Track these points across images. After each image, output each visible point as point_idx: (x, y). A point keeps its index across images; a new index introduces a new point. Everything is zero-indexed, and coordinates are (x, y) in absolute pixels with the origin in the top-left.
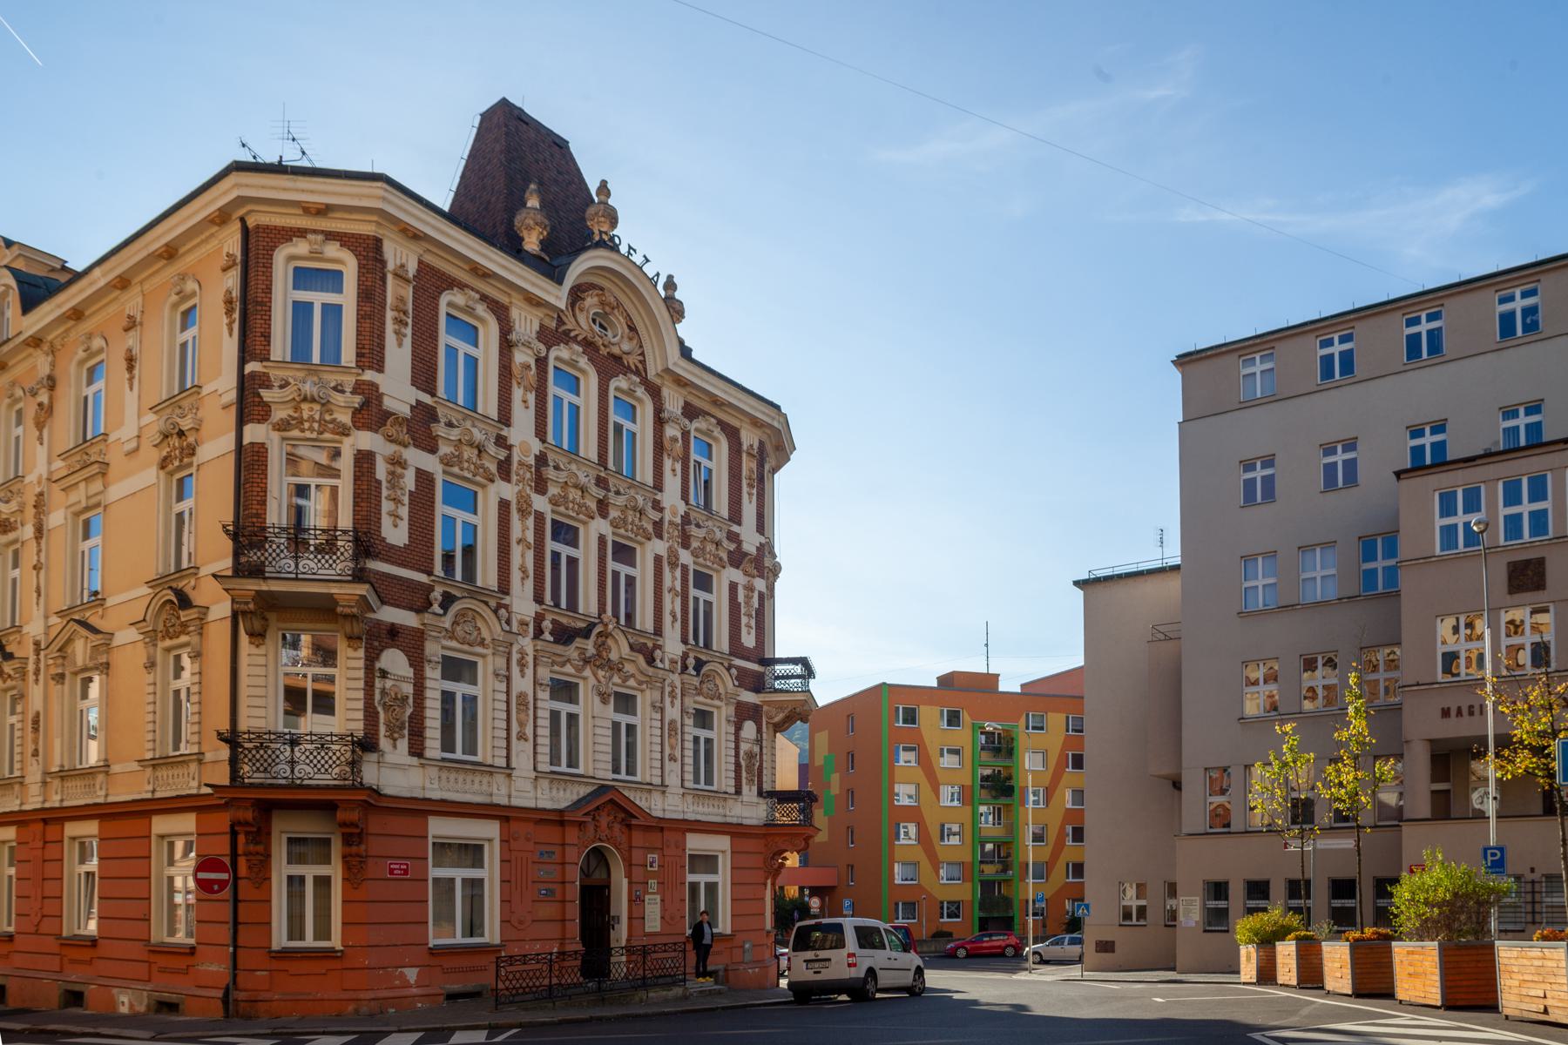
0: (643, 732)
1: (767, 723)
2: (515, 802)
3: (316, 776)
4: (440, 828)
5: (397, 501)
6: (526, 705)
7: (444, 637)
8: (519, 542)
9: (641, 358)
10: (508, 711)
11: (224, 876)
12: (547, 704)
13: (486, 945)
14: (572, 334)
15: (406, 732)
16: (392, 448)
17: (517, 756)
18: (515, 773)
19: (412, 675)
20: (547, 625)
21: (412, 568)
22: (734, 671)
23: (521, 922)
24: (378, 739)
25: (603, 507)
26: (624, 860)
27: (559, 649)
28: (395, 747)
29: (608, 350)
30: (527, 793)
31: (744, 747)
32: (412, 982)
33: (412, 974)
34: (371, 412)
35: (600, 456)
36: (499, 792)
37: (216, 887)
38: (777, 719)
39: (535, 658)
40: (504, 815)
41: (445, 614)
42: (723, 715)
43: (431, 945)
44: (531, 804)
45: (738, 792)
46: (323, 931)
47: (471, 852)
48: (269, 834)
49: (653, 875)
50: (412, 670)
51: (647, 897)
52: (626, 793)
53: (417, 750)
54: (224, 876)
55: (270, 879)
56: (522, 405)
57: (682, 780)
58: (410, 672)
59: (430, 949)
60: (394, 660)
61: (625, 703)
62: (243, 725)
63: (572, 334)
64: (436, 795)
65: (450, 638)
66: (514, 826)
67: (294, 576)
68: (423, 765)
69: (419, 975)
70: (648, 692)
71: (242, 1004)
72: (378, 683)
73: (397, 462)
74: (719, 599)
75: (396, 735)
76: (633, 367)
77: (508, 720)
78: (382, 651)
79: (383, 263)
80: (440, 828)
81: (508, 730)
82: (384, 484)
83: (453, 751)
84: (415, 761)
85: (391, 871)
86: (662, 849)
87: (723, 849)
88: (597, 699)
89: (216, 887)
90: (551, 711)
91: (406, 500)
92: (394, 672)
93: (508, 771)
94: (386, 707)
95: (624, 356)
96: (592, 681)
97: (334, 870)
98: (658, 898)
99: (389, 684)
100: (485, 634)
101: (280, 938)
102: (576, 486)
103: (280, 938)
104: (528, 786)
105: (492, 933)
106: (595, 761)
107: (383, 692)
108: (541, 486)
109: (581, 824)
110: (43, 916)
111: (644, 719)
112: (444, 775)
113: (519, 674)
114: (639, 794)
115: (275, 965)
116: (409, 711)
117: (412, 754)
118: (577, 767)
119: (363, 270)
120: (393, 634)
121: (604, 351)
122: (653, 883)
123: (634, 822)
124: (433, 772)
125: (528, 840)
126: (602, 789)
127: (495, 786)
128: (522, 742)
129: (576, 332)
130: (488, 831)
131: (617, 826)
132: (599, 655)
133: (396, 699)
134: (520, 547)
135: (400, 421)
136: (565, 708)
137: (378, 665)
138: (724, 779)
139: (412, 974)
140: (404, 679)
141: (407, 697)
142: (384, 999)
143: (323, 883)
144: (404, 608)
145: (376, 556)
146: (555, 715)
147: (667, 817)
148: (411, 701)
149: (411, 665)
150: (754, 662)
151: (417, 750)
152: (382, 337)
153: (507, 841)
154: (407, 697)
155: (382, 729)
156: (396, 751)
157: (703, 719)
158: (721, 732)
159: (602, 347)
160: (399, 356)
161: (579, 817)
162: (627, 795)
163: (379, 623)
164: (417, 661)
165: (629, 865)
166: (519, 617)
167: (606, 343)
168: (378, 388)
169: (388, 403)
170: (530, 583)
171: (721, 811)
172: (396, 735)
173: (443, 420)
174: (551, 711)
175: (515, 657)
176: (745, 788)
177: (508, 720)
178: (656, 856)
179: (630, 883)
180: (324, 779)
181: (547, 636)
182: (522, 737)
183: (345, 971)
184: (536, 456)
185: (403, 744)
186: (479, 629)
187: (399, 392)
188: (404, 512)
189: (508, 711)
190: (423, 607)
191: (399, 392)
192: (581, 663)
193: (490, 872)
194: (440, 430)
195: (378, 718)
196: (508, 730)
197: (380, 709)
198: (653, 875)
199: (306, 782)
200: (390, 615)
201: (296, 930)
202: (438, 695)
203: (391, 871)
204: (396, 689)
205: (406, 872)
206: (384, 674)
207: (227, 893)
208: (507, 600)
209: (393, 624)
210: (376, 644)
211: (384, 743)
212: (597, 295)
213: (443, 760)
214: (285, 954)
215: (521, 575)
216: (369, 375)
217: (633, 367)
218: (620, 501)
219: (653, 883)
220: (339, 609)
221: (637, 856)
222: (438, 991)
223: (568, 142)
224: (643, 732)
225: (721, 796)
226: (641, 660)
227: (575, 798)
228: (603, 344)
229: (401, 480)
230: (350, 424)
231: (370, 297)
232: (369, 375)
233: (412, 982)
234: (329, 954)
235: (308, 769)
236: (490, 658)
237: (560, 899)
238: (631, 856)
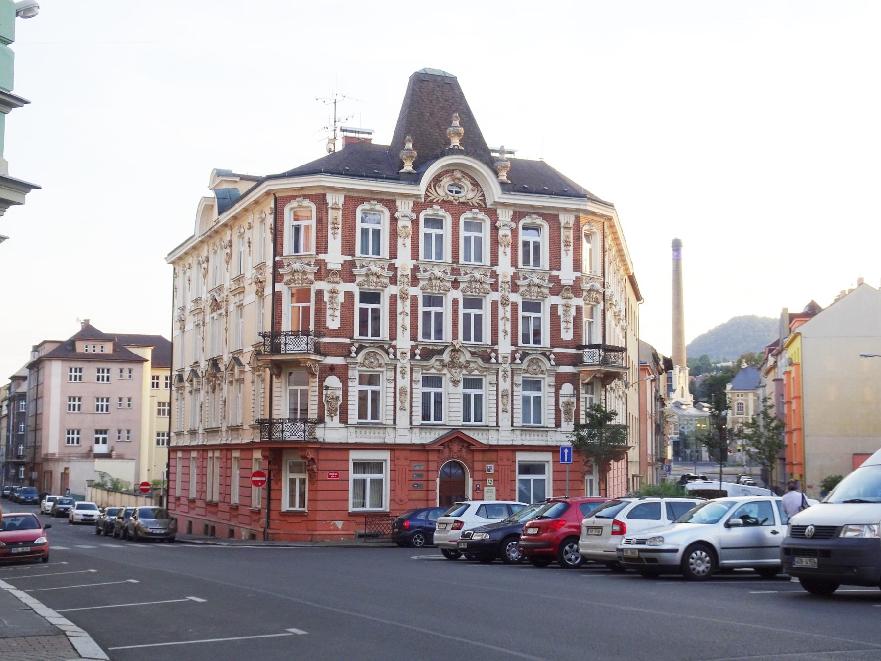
0: (486, 398)
1: (582, 384)
2: (398, 441)
3: (291, 437)
4: (521, 457)
5: (333, 309)
6: (405, 393)
7: (523, 373)
8: (401, 313)
9: (482, 198)
10: (497, 399)
11: (264, 479)
12: (520, 393)
13: (383, 512)
14: (434, 201)
15: (338, 413)
16: (564, 301)
17: (502, 420)
18: (500, 429)
19: (341, 387)
20: (418, 351)
21: (342, 337)
22: (552, 357)
23: (401, 501)
24: (324, 417)
25: (455, 284)
26: (470, 468)
27: (425, 363)
28: (332, 420)
29: (458, 201)
30: (404, 436)
31: (562, 400)
32: (340, 528)
33: (339, 524)
34: (557, 288)
35: (453, 257)
36: (389, 437)
37: (260, 484)
38: (587, 381)
39: (411, 370)
40: (393, 448)
41: (522, 363)
42: (548, 381)
43: (350, 511)
44: (408, 442)
45: (558, 425)
46: (302, 504)
47: (538, 468)
48: (281, 461)
49: (490, 476)
50: (341, 384)
51: (485, 488)
52: (467, 433)
53: (344, 419)
54: (264, 479)
55: (281, 480)
56: (503, 254)
57: (512, 422)
58: (340, 385)
59: (349, 513)
60: (333, 381)
61: (473, 383)
62: (274, 416)
63: (434, 201)
64: (519, 443)
65: (526, 372)
66: (398, 453)
67: (306, 351)
68: (347, 427)
69: (343, 525)
70: (487, 376)
71: (270, 535)
72: (324, 392)
73: (567, 306)
74: (545, 316)
75: (333, 415)
76: (476, 205)
77: (497, 404)
78: (326, 377)
79: (560, 224)
80: (521, 457)
81: (497, 408)
82: (328, 303)
83: (469, 420)
84: (342, 425)
85: (330, 477)
86: (497, 461)
87: (384, 458)
88: (451, 384)
89: (260, 484)
90: (464, 394)
91: (339, 307)
92: (332, 386)
93: (498, 428)
94: (328, 402)
95: (469, 201)
96: (449, 375)
97: (305, 476)
98: (494, 489)
99: (329, 392)
100: (543, 368)
101: (285, 506)
102: (436, 278)
103: (285, 506)
104: (406, 432)
105: (386, 507)
106: (453, 416)
107: (327, 396)
108: (415, 281)
109: (438, 451)
110: (226, 494)
111: (487, 392)
112: (359, 431)
113: (401, 377)
114: (476, 433)
115: (282, 518)
116: (339, 403)
117: (341, 422)
118: (441, 419)
119: (319, 210)
120: (332, 369)
121: (456, 203)
122: (490, 481)
123: (472, 448)
124: (353, 430)
125: (406, 459)
126: (455, 430)
127: (387, 434)
128: (505, 413)
129: (437, 199)
130: (385, 456)
131: (464, 450)
132: (452, 361)
133: (333, 398)
134: (402, 316)
135: (335, 273)
136: (532, 394)
137: (324, 384)
138: (548, 419)
139: (339, 524)
140: (338, 389)
141: (338, 397)
142: (324, 535)
143: (303, 482)
144: (338, 356)
145: (325, 336)
146: (526, 400)
147: (499, 444)
148: (341, 398)
149: (341, 382)
150: (573, 348)
151: (344, 419)
152: (327, 237)
153: (394, 460)
154: (338, 397)
155: (326, 412)
156: (334, 422)
157: (535, 385)
158: (546, 393)
159: (454, 201)
160: (335, 243)
161: (436, 447)
162: (468, 434)
163: (325, 365)
164: (345, 380)
165: (473, 470)
166: (401, 350)
167: (456, 198)
168: (325, 261)
169: (563, 282)
170: (509, 337)
171: (544, 438)
172: (333, 415)
173: (522, 277)
174: (464, 394)
175: (399, 370)
176: (564, 424)
177: (497, 404)
178: (493, 465)
179: (473, 480)
180: (293, 438)
181: (418, 357)
182: (504, 411)
183: (309, 522)
184: (411, 269)
185: (337, 418)
186: (378, 360)
187: (335, 258)
188: (338, 313)
189: (497, 399)
190: (348, 355)
191: (567, 275)
192: (441, 367)
193: (385, 476)
194: (356, 271)
195: (324, 408)
196: (497, 408)
197: (325, 404)
198: (490, 476)
199: (287, 439)
200: (331, 360)
201: (292, 504)
202: (521, 398)
203: (330, 477)
204: (333, 394)
205: (337, 477)
206: (327, 388)
207: (265, 485)
208: (496, 347)
209: (332, 365)
210: (324, 374)
211: (327, 419)
212: (449, 176)
213: (523, 427)
214: (288, 514)
215: (504, 334)
216: (554, 273)
217: (476, 205)
218: (467, 278)
219: (490, 481)
220: (302, 365)
221: (478, 466)
222: (353, 532)
223: (13, 54)
224: (486, 398)
225: (545, 430)
226: (480, 361)
227: (437, 436)
228: (454, 199)
229: (336, 299)
230: (313, 279)
231: (321, 222)
232: (554, 273)
233: (340, 528)
234: (300, 514)
235: (288, 434)
236: (385, 372)
237: (425, 489)
238: (473, 466)
